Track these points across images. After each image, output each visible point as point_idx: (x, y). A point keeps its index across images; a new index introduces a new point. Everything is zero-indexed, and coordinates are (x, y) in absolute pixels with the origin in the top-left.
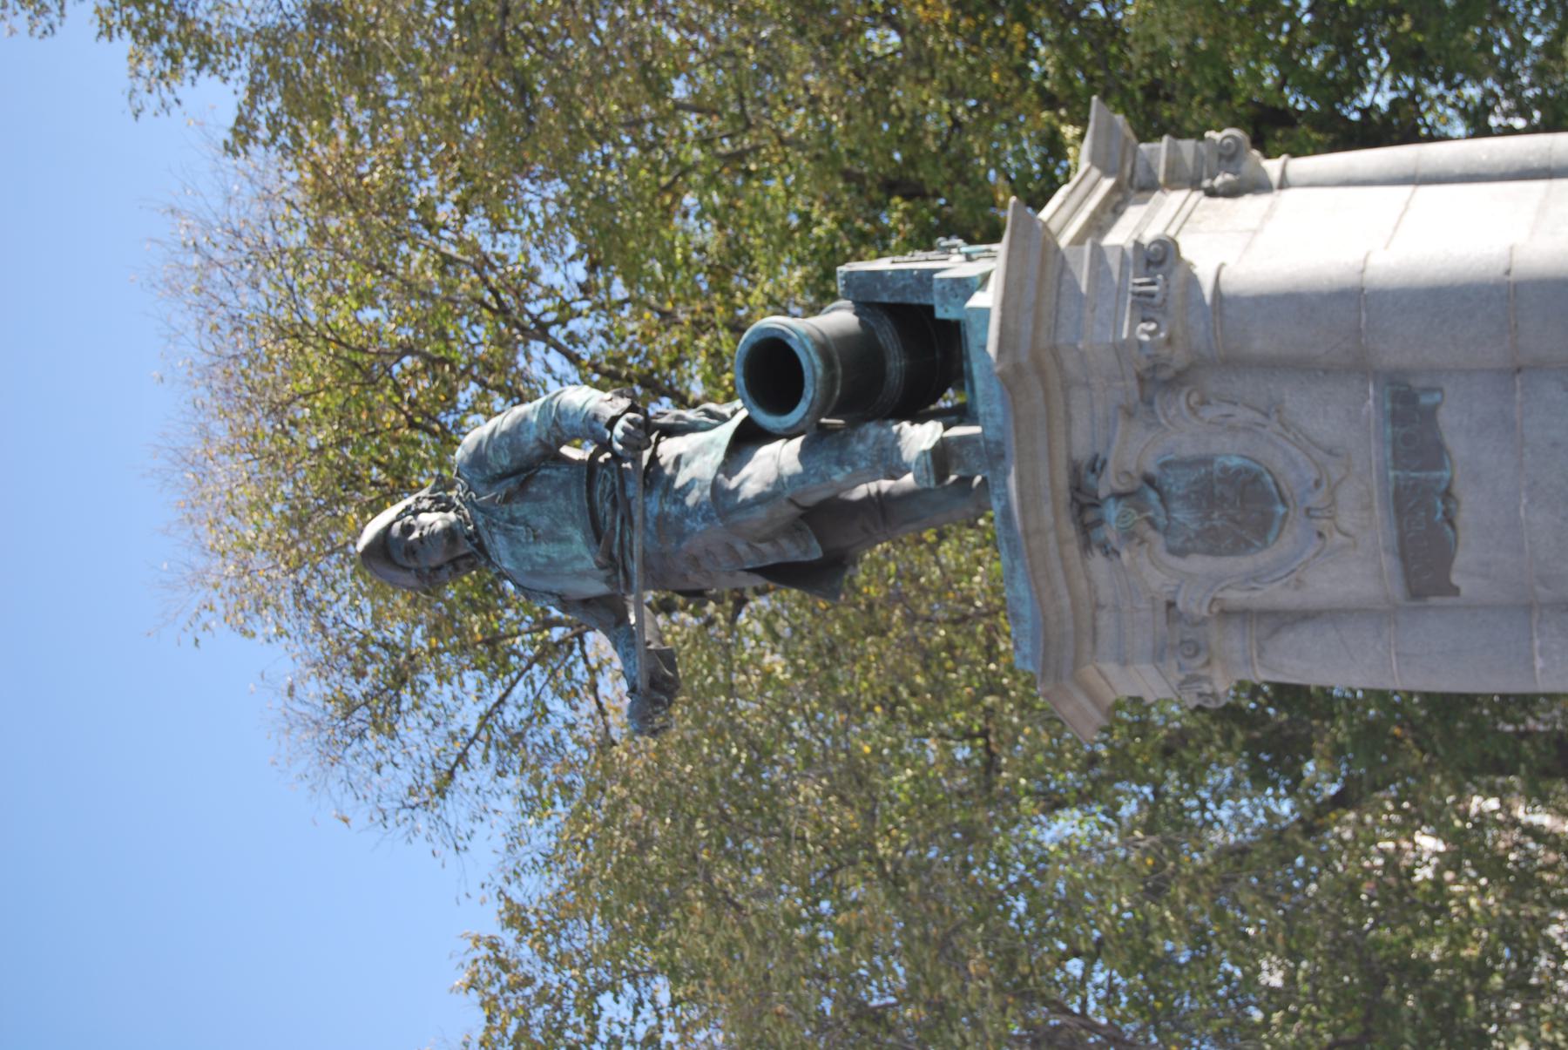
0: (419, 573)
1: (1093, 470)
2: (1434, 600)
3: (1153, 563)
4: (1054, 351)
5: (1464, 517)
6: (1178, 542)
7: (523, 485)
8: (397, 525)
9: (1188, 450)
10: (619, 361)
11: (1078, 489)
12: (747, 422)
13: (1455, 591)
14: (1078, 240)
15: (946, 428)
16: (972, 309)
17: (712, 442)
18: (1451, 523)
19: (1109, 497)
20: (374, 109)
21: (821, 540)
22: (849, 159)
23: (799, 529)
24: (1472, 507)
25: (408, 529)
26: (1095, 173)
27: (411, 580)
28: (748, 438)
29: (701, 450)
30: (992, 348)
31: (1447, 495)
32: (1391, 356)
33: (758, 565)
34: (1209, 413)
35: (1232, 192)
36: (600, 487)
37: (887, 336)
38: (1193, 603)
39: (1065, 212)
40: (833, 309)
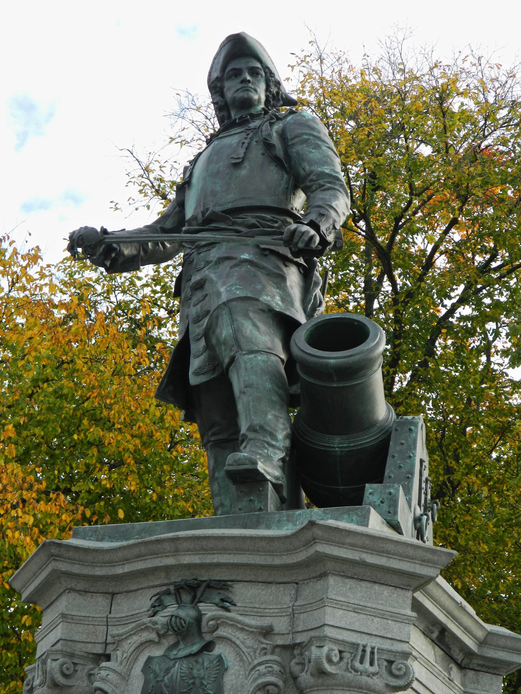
1: (223, 600)
3: (142, 644)
4: (324, 575)
6: (155, 666)
7: (277, 160)
8: (258, 65)
10: (511, 431)
11: (209, 586)
12: (296, 324)
14: (417, 606)
15: (277, 487)
16: (369, 511)
17: (292, 304)
19: (199, 611)
22: (234, 69)
23: (214, 370)
25: (254, 72)
26: (480, 634)
29: (287, 298)
30: (331, 522)
33: (191, 337)
36: (268, 216)
39: (448, 603)
40: (388, 408)
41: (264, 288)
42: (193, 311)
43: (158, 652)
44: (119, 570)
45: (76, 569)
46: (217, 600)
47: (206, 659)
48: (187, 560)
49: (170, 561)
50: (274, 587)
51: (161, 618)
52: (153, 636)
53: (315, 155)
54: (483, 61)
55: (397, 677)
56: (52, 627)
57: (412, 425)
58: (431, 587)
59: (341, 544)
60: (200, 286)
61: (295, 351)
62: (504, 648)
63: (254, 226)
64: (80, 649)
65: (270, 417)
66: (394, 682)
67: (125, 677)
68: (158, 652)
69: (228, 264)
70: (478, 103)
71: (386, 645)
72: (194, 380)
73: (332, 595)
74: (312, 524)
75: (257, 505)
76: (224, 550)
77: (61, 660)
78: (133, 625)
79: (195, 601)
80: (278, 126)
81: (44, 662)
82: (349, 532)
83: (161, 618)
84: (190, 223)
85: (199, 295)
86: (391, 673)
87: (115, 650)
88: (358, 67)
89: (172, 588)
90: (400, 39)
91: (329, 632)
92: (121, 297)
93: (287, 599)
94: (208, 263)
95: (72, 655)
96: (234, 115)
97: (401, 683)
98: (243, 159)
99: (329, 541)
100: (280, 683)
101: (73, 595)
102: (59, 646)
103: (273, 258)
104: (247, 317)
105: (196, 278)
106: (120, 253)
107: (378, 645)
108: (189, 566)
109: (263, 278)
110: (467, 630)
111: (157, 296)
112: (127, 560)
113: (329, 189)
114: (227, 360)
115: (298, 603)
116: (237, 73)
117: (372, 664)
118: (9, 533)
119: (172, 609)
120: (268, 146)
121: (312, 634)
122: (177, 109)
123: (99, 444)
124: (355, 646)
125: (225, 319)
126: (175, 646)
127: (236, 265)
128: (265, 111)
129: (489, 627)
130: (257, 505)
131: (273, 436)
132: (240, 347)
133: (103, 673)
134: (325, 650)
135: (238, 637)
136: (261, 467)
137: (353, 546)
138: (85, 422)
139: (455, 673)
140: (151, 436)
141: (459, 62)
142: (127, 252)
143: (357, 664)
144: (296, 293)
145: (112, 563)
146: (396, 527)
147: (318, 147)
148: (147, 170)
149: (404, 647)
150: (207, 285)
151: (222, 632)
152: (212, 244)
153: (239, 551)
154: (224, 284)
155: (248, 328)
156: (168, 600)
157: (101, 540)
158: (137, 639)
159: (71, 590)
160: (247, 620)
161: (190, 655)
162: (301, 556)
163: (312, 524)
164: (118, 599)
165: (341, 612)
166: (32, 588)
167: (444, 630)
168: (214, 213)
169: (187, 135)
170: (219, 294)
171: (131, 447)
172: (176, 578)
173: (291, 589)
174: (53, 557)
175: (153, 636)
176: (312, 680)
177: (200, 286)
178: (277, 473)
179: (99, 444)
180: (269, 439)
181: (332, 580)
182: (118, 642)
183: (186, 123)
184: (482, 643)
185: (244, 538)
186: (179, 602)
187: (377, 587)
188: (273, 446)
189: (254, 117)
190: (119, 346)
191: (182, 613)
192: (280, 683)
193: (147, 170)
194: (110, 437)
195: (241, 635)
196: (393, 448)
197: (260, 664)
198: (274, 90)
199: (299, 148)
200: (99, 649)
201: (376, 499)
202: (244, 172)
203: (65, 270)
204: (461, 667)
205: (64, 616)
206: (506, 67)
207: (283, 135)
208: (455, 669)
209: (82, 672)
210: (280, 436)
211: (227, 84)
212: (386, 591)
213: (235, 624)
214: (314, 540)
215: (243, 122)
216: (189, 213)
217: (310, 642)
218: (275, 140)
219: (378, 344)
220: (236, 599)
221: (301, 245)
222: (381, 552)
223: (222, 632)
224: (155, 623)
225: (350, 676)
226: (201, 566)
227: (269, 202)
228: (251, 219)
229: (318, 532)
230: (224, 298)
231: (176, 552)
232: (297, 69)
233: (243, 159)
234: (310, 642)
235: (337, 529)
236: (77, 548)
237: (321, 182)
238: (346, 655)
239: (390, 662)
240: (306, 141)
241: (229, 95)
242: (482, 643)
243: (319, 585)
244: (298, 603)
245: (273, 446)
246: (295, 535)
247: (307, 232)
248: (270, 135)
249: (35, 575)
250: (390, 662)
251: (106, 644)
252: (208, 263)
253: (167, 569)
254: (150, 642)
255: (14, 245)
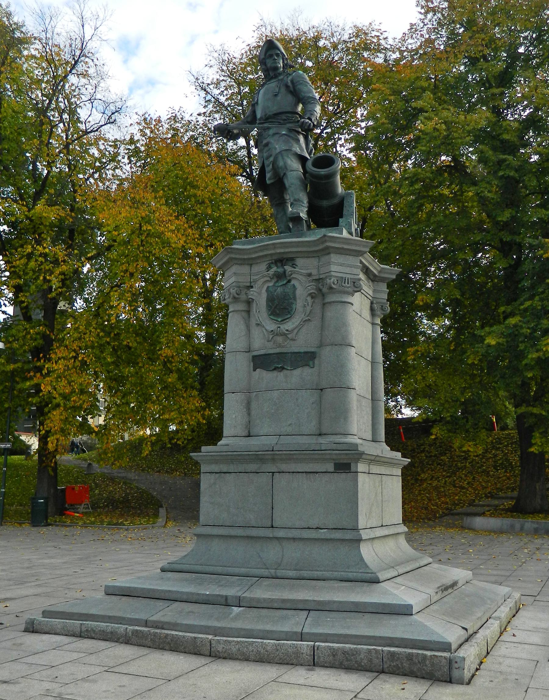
1: (293, 265)
4: (329, 253)
7: (291, 92)
11: (287, 260)
14: (361, 262)
25: (278, 55)
26: (379, 269)
30: (330, 234)
41: (292, 145)
43: (271, 284)
45: (237, 256)
46: (291, 265)
47: (289, 285)
48: (278, 251)
49: (272, 252)
50: (311, 259)
51: (271, 272)
52: (268, 279)
54: (332, 24)
55: (357, 287)
57: (350, 195)
59: (335, 242)
60: (267, 145)
61: (308, 169)
63: (285, 120)
64: (241, 284)
65: (301, 195)
66: (356, 289)
67: (259, 294)
68: (271, 284)
69: (277, 136)
70: (331, 43)
71: (352, 277)
72: (268, 182)
73: (332, 260)
74: (325, 236)
75: (300, 229)
77: (236, 289)
78: (260, 275)
79: (283, 266)
80: (290, 78)
81: (229, 290)
83: (271, 272)
85: (266, 149)
87: (255, 284)
89: (273, 261)
90: (297, 16)
91: (333, 274)
92: (191, 133)
93: (316, 263)
94: (269, 135)
95: (239, 287)
96: (272, 74)
97: (358, 289)
98: (278, 93)
99: (331, 241)
100: (316, 292)
101: (237, 266)
102: (234, 284)
103: (294, 132)
104: (288, 157)
105: (265, 142)
106: (233, 133)
107: (349, 277)
108: (280, 253)
109: (291, 141)
110: (375, 268)
111: (205, 131)
112: (256, 252)
113: (313, 103)
114: (282, 174)
115: (320, 264)
116: (271, 56)
117: (348, 284)
118: (167, 234)
120: (287, 86)
121: (327, 274)
122: (207, 52)
125: (280, 158)
126: (277, 281)
127: (281, 136)
128: (284, 71)
129: (382, 266)
130: (300, 229)
131: (303, 203)
132: (287, 169)
133: (252, 293)
134: (332, 280)
135: (300, 277)
136: (301, 215)
137: (339, 242)
138: (188, 187)
140: (213, 191)
141: (322, 25)
143: (343, 284)
144: (304, 146)
146: (351, 234)
147: (306, 86)
148: (197, 79)
150: (269, 145)
151: (293, 276)
152: (269, 128)
154: (277, 144)
155: (289, 162)
156: (272, 266)
157: (244, 245)
160: (302, 271)
161: (283, 285)
162: (321, 247)
163: (325, 236)
164: (253, 266)
165: (336, 266)
168: (269, 116)
169: (212, 63)
170: (276, 149)
171: (207, 196)
172: (275, 257)
174: (229, 253)
175: (268, 279)
176: (327, 291)
178: (306, 216)
179: (195, 196)
180: (301, 204)
181: (332, 255)
182: (255, 281)
183: (211, 58)
187: (348, 256)
188: (303, 206)
189: (280, 74)
190: (199, 156)
191: (279, 270)
192: (316, 292)
193: (197, 79)
194: (199, 193)
195: (301, 277)
197: (309, 286)
198: (286, 62)
199: (299, 86)
200: (248, 284)
201: (344, 224)
202: (279, 98)
203: (168, 123)
204: (372, 281)
205: (235, 273)
207: (292, 81)
208: (370, 281)
209: (243, 292)
210: (305, 202)
212: (351, 258)
213: (298, 273)
214: (326, 241)
215: (276, 76)
216: (259, 115)
218: (290, 84)
219: (339, 165)
220: (297, 264)
221: (306, 127)
222: (348, 244)
223: (293, 276)
224: (269, 274)
225: (341, 288)
226: (284, 253)
227: (289, 109)
228: (284, 117)
230: (278, 150)
231: (275, 248)
232: (256, 32)
233: (278, 93)
234: (326, 277)
235: (333, 237)
236: (237, 249)
237: (309, 100)
238: (339, 281)
239: (354, 283)
240: (302, 83)
241: (269, 65)
242: (380, 272)
243: (327, 257)
244: (320, 264)
245: (303, 206)
246: (318, 240)
247: (308, 122)
248: (287, 82)
249: (222, 259)
250: (354, 283)
251: (251, 282)
252: (269, 135)
253: (271, 255)
254: (268, 281)
255: (150, 116)
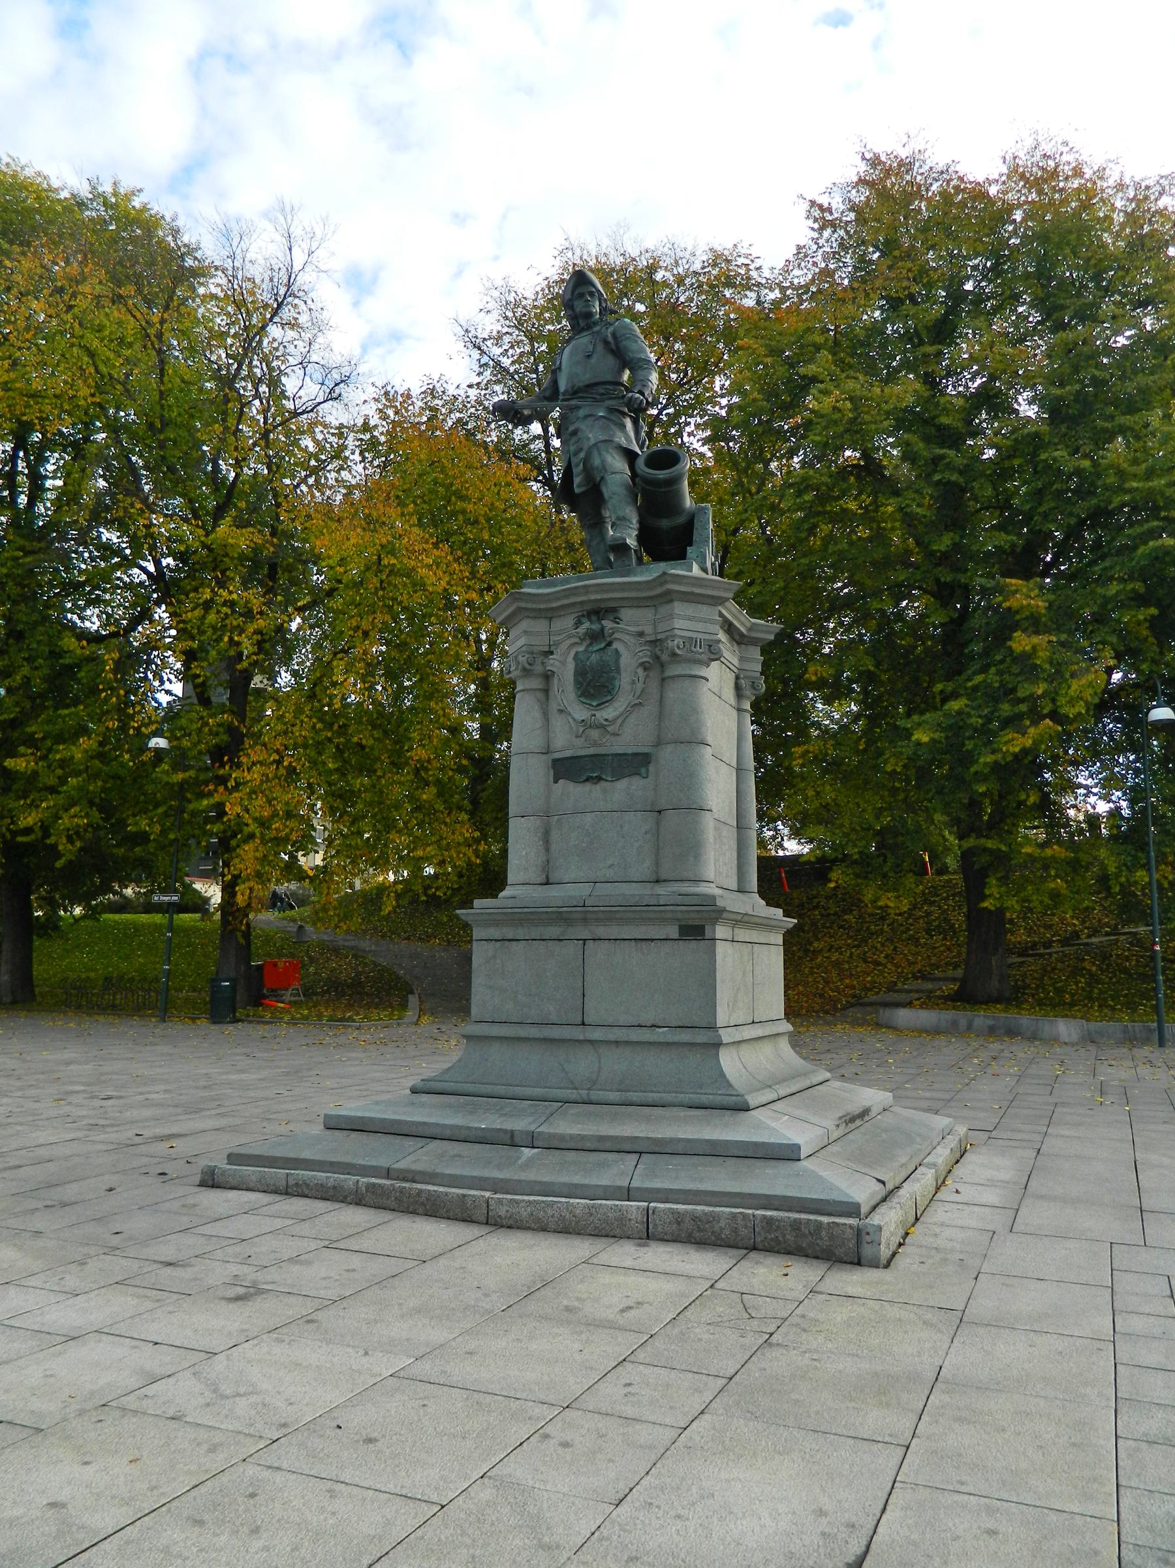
0: (570, 300)
2: (552, 773)
4: (671, 601)
5: (588, 787)
9: (623, 661)
13: (556, 782)
14: (721, 615)
18: (587, 780)
20: (793, 694)
21: (583, 493)
24: (594, 792)
25: (591, 294)
26: (748, 625)
27: (568, 296)
28: (630, 456)
30: (673, 571)
31: (599, 779)
32: (666, 754)
34: (640, 671)
35: (738, 688)
37: (681, 520)
38: (553, 663)
42: (572, 448)
43: (581, 649)
44: (554, 605)
45: (529, 606)
47: (610, 651)
48: (593, 597)
52: (577, 640)
53: (634, 347)
56: (517, 638)
58: (727, 604)
59: (680, 584)
62: (761, 631)
63: (603, 394)
64: (536, 649)
67: (564, 663)
68: (581, 649)
71: (707, 637)
72: (577, 490)
73: (676, 611)
74: (664, 574)
76: (613, 591)
79: (599, 620)
80: (611, 329)
82: (684, 576)
83: (582, 630)
84: (564, 394)
85: (574, 439)
86: (710, 651)
88: (594, 253)
91: (677, 632)
92: (458, 415)
95: (532, 653)
96: (582, 323)
99: (674, 582)
102: (524, 649)
104: (607, 451)
105: (571, 428)
106: (522, 414)
109: (613, 427)
110: (742, 624)
112: (559, 599)
116: (582, 295)
119: (586, 625)
123: (464, 512)
124: (691, 638)
125: (595, 453)
126: (591, 644)
129: (753, 620)
135: (626, 638)
137: (687, 584)
138: (453, 498)
139: (736, 647)
140: (492, 504)
142: (526, 412)
144: (632, 434)
145: (549, 601)
147: (636, 342)
148: (467, 331)
149: (714, 637)
151: (616, 635)
153: (623, 590)
155: (609, 459)
156: (584, 620)
158: (569, 642)
159: (528, 617)
160: (630, 628)
162: (658, 591)
163: (664, 574)
164: (554, 620)
166: (503, 617)
167: (730, 624)
169: (490, 306)
170: (589, 439)
172: (588, 607)
173: (652, 610)
174: (516, 600)
175: (577, 640)
177: (575, 433)
181: (676, 604)
182: (557, 644)
183: (489, 299)
184: (750, 630)
185: (624, 583)
186: (590, 620)
189: (595, 324)
191: (594, 627)
193: (467, 331)
194: (470, 507)
196: (697, 524)
199: (624, 343)
200: (546, 649)
202: (593, 360)
204: (738, 643)
206: (690, 249)
207: (614, 335)
209: (539, 661)
211: (576, 303)
212: (705, 607)
213: (623, 631)
215: (588, 327)
216: (562, 388)
217: (667, 638)
218: (610, 339)
222: (701, 586)
223: (616, 635)
225: (690, 655)
227: (609, 378)
228: (601, 390)
229: (669, 578)
230: (592, 441)
231: (587, 593)
234: (667, 638)
235: (678, 575)
239: (710, 646)
241: (578, 310)
242: (750, 630)
243: (668, 607)
246: (654, 580)
249: (505, 610)
250: (710, 646)
253: (582, 603)
